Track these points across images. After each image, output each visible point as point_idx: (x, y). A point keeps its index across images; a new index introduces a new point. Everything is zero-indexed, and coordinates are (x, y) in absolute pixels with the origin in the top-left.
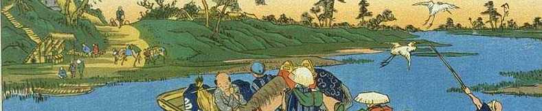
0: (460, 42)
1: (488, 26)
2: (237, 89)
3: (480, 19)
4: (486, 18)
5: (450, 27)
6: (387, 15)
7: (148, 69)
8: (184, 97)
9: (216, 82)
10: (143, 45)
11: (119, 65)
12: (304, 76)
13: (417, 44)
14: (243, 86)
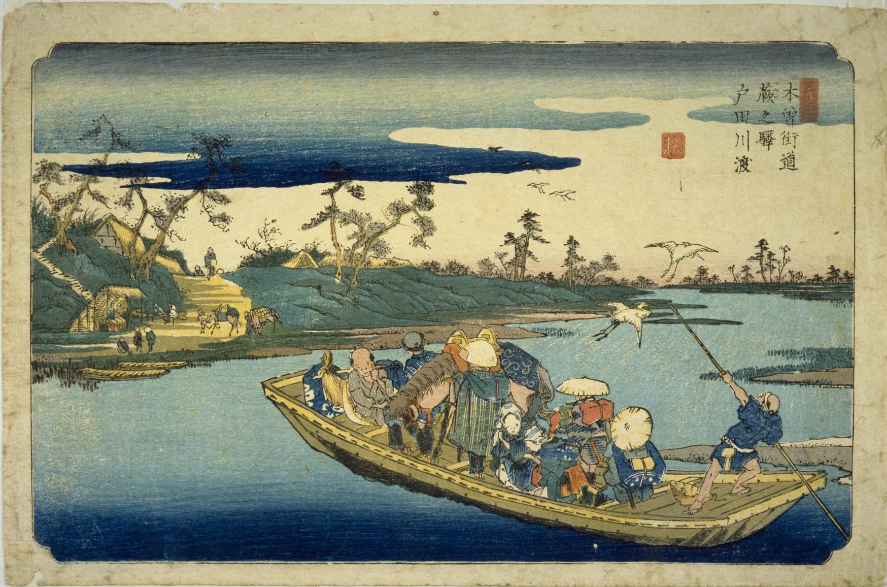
0: (719, 305)
1: (758, 278)
2: (383, 373)
3: (746, 268)
4: (755, 266)
5: (705, 284)
6: (715, 277)
7: (465, 416)
8: (304, 382)
9: (352, 361)
10: (244, 305)
11: (207, 333)
12: (481, 353)
13: (652, 304)
14: (394, 370)
